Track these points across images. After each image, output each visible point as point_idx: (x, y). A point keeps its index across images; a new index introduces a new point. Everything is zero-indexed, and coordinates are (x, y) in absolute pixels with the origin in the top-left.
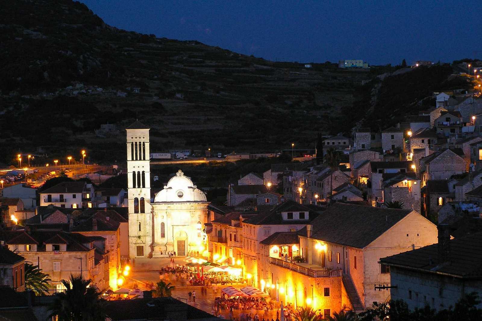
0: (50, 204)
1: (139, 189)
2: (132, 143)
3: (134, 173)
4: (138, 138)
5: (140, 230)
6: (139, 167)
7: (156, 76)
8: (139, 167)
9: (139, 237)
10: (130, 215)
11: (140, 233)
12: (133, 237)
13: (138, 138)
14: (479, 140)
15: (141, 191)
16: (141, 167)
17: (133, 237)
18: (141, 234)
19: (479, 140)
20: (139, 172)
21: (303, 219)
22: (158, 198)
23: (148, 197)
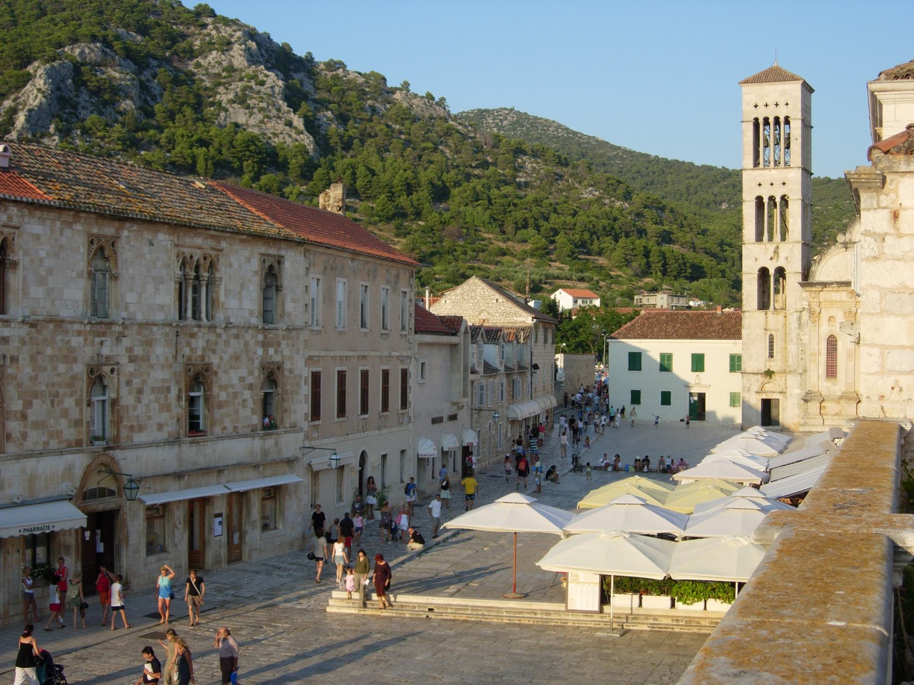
0: (764, 201)
1: (771, 247)
2: (756, 120)
3: (759, 200)
4: (772, 107)
5: (239, 559)
6: (772, 184)
7: (128, 102)
8: (772, 184)
9: (769, 373)
10: (747, 314)
11: (772, 363)
12: (753, 374)
13: (772, 107)
14: (401, 646)
15: (776, 252)
16: (766, 185)
17: (753, 374)
18: (774, 365)
19: (401, 646)
20: (772, 198)
21: (551, 599)
22: (826, 269)
23: (794, 268)
